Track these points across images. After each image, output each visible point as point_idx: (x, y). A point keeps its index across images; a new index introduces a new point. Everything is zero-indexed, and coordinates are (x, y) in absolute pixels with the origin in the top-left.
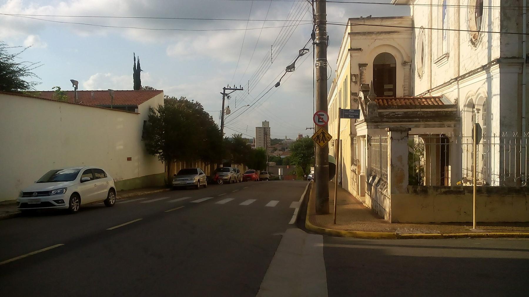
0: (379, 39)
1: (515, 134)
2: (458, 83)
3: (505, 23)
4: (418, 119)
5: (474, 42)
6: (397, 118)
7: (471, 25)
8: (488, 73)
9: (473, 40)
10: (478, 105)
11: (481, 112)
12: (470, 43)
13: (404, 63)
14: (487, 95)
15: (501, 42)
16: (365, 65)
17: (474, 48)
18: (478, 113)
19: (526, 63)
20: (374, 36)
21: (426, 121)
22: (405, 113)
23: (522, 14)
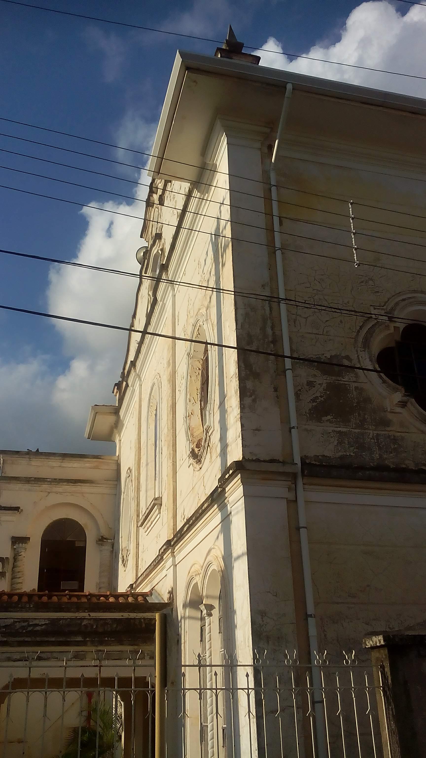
0: (57, 493)
1: (292, 655)
2: (173, 552)
3: (249, 384)
4: (79, 639)
5: (196, 456)
6: (34, 633)
7: (193, 425)
8: (223, 507)
9: (196, 450)
10: (207, 597)
11: (216, 613)
12: (192, 461)
13: (101, 540)
14: (222, 564)
15: (242, 426)
16: (25, 540)
17: (198, 467)
18: (210, 615)
19: (303, 475)
20: (45, 486)
21: (101, 643)
22: (54, 621)
23: (284, 371)
